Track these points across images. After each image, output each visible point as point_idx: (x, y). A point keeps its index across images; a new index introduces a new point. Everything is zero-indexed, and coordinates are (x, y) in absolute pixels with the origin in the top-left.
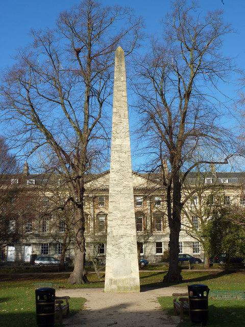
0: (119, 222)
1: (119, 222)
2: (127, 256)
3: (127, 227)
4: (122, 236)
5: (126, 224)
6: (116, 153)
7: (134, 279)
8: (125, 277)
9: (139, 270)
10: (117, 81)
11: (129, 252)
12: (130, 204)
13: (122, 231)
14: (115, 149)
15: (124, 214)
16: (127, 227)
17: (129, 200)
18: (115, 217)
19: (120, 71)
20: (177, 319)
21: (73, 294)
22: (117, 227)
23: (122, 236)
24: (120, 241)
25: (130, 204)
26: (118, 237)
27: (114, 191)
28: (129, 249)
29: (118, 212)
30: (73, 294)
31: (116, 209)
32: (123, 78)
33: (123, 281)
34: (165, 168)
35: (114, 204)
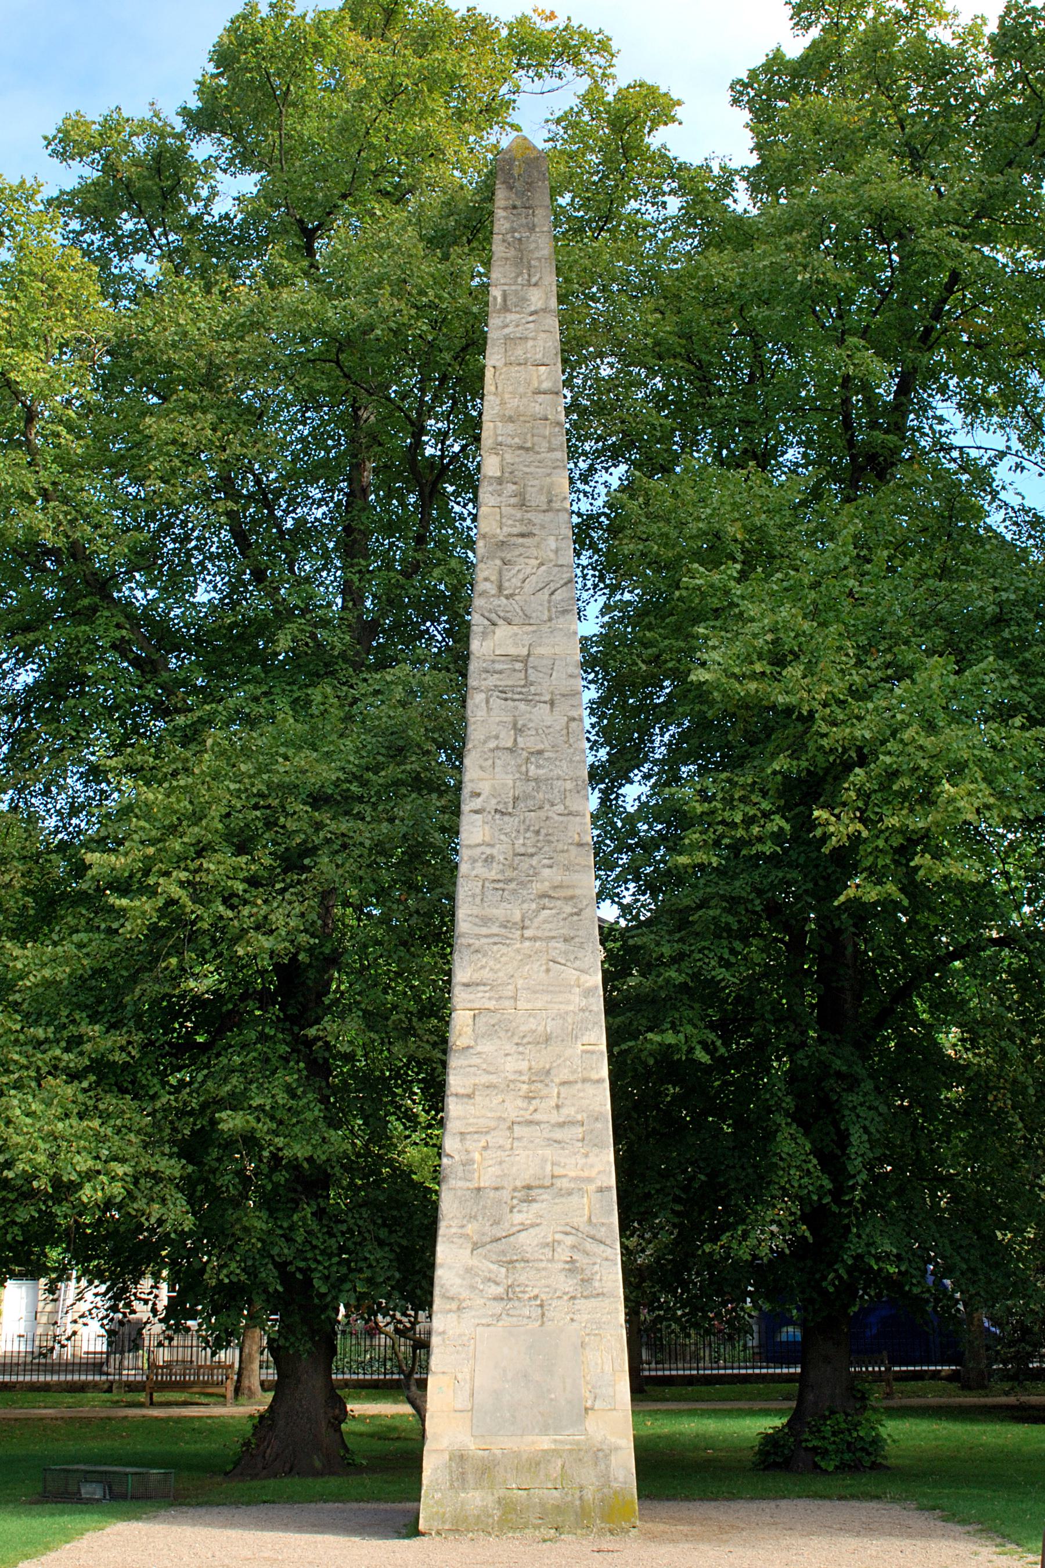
0: (514, 1108)
1: (514, 1108)
2: (558, 1311)
3: (558, 1135)
4: (528, 1193)
5: (555, 1117)
6: (496, 703)
7: (600, 1455)
8: (545, 1443)
9: (642, 1387)
10: (505, 308)
11: (567, 1284)
12: (576, 1000)
13: (527, 1162)
14: (492, 681)
15: (542, 1058)
16: (558, 1135)
17: (571, 974)
18: (485, 1079)
19: (522, 261)
20: (948, 8)
21: (842, 898)
22: (499, 1138)
23: (528, 1193)
24: (518, 1218)
25: (576, 1000)
26: (505, 1194)
27: (486, 921)
28: (572, 1268)
29: (510, 1048)
30: (842, 898)
31: (498, 1027)
32: (543, 296)
33: (536, 1463)
34: (301, 705)
35: (480, 998)
